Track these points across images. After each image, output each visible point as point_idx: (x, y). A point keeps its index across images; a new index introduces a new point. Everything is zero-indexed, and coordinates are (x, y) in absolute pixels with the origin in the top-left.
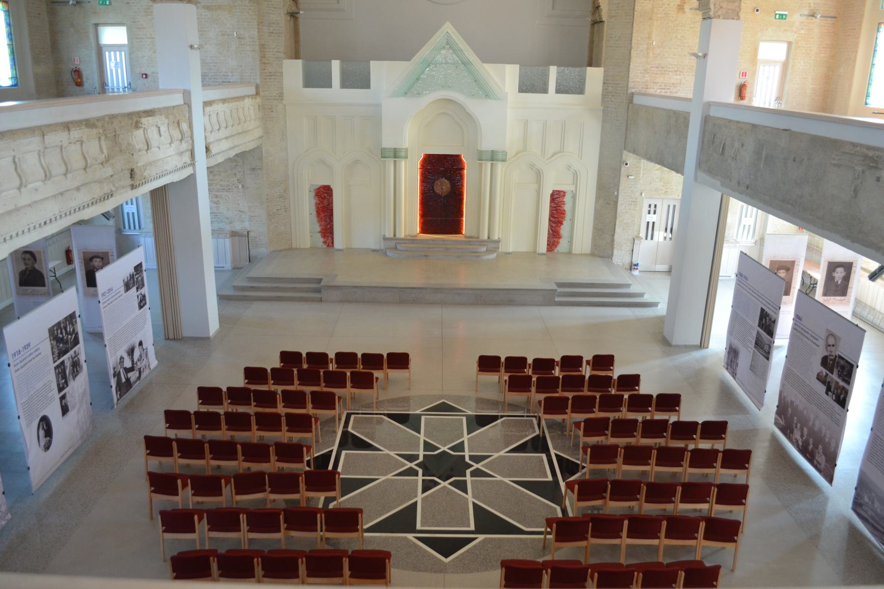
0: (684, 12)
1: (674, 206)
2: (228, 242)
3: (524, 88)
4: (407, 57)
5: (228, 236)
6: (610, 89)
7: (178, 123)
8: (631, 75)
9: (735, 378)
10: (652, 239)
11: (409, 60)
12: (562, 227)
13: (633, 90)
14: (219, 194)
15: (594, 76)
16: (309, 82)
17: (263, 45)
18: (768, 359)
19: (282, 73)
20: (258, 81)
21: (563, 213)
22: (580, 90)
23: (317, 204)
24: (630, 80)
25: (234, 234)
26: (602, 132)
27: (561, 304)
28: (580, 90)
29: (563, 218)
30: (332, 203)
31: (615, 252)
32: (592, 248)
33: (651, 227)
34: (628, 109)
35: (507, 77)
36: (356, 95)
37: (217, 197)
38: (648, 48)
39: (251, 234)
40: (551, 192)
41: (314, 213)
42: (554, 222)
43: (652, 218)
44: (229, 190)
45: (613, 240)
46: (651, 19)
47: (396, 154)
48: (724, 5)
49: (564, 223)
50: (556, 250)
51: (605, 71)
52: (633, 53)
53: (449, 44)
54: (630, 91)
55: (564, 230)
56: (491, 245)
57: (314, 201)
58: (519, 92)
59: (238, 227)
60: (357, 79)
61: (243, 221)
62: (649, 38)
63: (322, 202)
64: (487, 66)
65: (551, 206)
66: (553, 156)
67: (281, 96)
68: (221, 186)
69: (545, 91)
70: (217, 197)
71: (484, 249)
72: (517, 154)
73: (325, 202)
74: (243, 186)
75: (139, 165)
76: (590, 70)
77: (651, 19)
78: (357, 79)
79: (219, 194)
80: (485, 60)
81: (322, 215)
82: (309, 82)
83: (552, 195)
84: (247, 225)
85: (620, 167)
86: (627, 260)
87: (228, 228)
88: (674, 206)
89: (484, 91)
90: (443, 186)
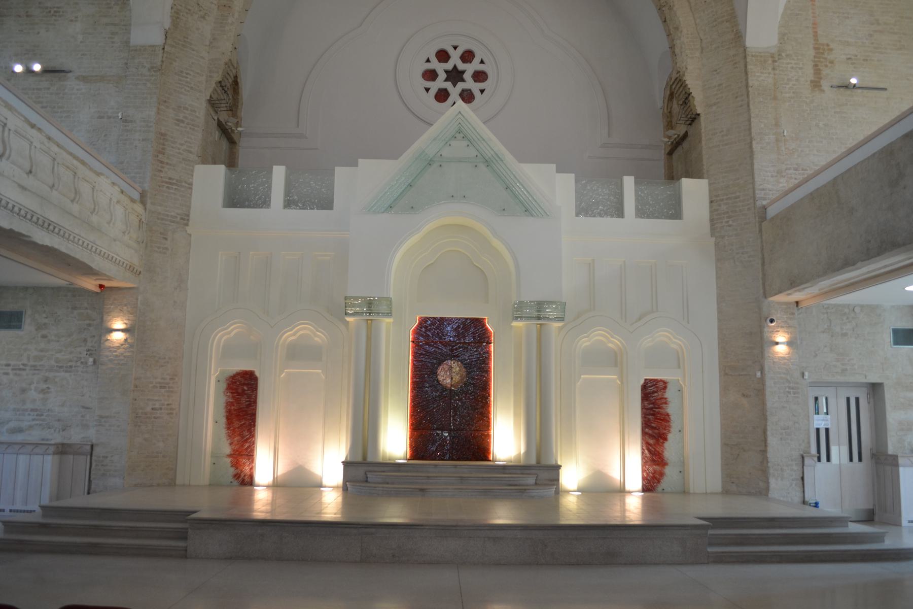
0: (823, 91)
1: (857, 399)
2: (49, 462)
3: (584, 209)
4: (396, 157)
5: (52, 449)
6: (724, 208)
10: (828, 460)
11: (397, 159)
12: (666, 444)
13: (764, 203)
14: (51, 375)
15: (694, 192)
16: (235, 199)
17: (162, 134)
19: (191, 184)
20: (147, 186)
22: (674, 211)
23: (229, 404)
24: (757, 186)
25: (63, 450)
26: (718, 278)
27: (720, 559)
28: (674, 211)
29: (668, 428)
30: (255, 402)
31: (772, 481)
32: (724, 482)
33: (824, 438)
34: (760, 231)
35: (556, 188)
36: (309, 219)
37: (46, 380)
38: (777, 140)
39: (97, 450)
40: (642, 382)
41: (223, 421)
42: (651, 436)
43: (820, 421)
46: (775, 98)
47: (372, 308)
49: (670, 437)
50: (659, 488)
51: (710, 184)
53: (461, 133)
54: (759, 203)
55: (670, 450)
56: (544, 475)
57: (223, 400)
58: (577, 215)
59: (75, 436)
60: (312, 196)
62: (777, 125)
63: (238, 401)
64: (523, 165)
65: (643, 408)
66: (640, 319)
67: (185, 219)
68: (57, 361)
69: (619, 212)
70: (46, 380)
71: (531, 480)
73: (244, 400)
74: (95, 362)
76: (687, 183)
77: (775, 98)
78: (312, 196)
79: (51, 375)
81: (237, 424)
82: (235, 199)
83: (644, 387)
84: (92, 434)
87: (57, 438)
88: (857, 399)
90: (450, 374)
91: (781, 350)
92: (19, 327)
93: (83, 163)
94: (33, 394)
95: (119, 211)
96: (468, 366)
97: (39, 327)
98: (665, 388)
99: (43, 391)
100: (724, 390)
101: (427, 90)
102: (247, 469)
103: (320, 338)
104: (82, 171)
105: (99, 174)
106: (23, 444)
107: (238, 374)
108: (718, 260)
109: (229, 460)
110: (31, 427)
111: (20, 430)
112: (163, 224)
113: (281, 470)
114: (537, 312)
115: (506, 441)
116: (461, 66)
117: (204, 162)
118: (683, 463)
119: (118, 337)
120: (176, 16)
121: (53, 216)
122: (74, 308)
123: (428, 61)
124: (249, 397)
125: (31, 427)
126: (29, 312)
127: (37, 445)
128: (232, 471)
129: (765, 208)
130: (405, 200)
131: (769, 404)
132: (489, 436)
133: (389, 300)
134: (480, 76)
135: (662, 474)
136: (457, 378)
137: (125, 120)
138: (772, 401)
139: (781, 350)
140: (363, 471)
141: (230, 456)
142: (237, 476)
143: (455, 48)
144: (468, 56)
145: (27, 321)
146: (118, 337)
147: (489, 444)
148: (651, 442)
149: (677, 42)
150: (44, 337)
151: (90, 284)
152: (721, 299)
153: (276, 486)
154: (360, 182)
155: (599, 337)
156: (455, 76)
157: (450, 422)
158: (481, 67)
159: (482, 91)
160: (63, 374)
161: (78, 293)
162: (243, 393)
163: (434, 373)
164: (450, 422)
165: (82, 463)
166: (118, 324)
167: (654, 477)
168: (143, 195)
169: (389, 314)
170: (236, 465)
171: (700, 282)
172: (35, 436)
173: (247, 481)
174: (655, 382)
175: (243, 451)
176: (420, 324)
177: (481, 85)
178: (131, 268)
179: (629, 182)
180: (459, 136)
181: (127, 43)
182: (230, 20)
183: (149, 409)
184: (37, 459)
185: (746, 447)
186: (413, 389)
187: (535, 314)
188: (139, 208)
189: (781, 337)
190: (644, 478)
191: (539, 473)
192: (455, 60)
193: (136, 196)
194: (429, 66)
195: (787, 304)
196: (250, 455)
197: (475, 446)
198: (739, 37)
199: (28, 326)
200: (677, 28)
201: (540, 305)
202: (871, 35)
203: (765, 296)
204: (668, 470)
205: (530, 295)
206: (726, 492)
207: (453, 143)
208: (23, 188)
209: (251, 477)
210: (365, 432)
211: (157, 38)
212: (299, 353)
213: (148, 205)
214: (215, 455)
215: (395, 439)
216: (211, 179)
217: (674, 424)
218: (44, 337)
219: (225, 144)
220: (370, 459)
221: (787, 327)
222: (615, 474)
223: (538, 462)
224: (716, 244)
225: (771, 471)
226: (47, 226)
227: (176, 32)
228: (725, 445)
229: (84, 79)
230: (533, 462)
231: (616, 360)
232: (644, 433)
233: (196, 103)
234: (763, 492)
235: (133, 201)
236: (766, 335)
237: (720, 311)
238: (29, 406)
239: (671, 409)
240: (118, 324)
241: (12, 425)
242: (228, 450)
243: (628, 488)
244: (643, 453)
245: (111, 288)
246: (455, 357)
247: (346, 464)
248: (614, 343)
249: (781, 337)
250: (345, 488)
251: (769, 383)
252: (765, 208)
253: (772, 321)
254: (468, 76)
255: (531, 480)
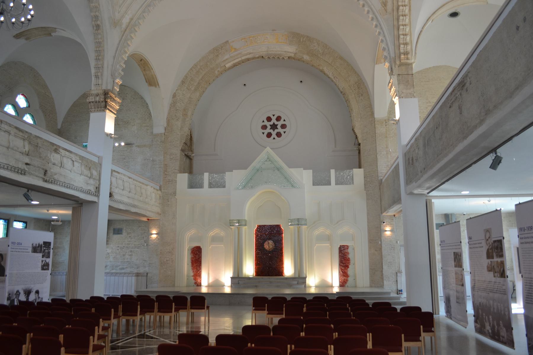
2: (134, 278)
4: (246, 168)
5: (134, 275)
7: (90, 168)
8: (379, 169)
9: (451, 318)
12: (349, 269)
16: (191, 186)
18: (463, 285)
20: (161, 183)
21: (348, 260)
22: (351, 181)
23: (192, 258)
25: (138, 275)
26: (367, 206)
28: (351, 181)
29: (349, 263)
30: (201, 257)
31: (385, 282)
34: (380, 189)
35: (305, 176)
37: (131, 251)
38: (387, 153)
40: (339, 246)
41: (190, 264)
42: (343, 266)
44: (138, 248)
45: (382, 275)
46: (386, 137)
48: (404, 91)
49: (350, 266)
50: (346, 285)
52: (379, 157)
53: (269, 159)
54: (380, 178)
55: (350, 271)
56: (300, 281)
57: (190, 256)
58: (313, 185)
59: (141, 270)
61: (145, 267)
62: (387, 147)
63: (195, 257)
64: (291, 169)
67: (175, 194)
69: (329, 183)
70: (131, 251)
71: (296, 282)
72: (314, 223)
73: (197, 256)
75: (52, 170)
80: (290, 167)
81: (195, 265)
82: (191, 186)
83: (340, 248)
84: (147, 269)
85: (380, 225)
86: (394, 288)
87: (135, 271)
89: (290, 183)
90: (269, 245)
91: (388, 233)
92: (121, 234)
93: (143, 184)
94: (127, 256)
95: (153, 195)
96: (275, 242)
97: (128, 234)
98: (348, 248)
99: (130, 255)
100: (370, 248)
101: (263, 133)
102: (199, 281)
103: (222, 234)
104: (143, 186)
105: (147, 185)
106: (125, 273)
107: (195, 247)
108: (367, 199)
109: (193, 278)
110: (127, 268)
111: (123, 269)
112: (167, 197)
113: (211, 281)
114: (299, 222)
115: (288, 269)
116: (276, 123)
117: (180, 173)
118: (355, 276)
119: (154, 236)
120: (168, 121)
121: (136, 203)
122: (139, 227)
123: (263, 122)
124: (199, 255)
125: (127, 268)
126: (125, 228)
127: (130, 273)
128: (194, 281)
129: (382, 180)
130: (249, 184)
131: (383, 254)
132: (283, 267)
133: (245, 220)
134: (284, 126)
135: (347, 280)
136: (271, 247)
137: (153, 161)
138: (384, 253)
139: (388, 233)
140: (238, 280)
141: (193, 276)
142: (196, 283)
143: (274, 115)
144: (278, 119)
145: (124, 231)
146: (154, 236)
147: (283, 270)
148: (343, 268)
149: (352, 115)
150: (130, 237)
151: (145, 219)
152: (368, 214)
153: (209, 286)
154: (234, 178)
155: (320, 231)
156: (274, 127)
157: (269, 263)
158: (284, 123)
159: (285, 132)
160: (136, 249)
161: (140, 221)
162: (196, 254)
163: (262, 245)
164: (269, 263)
165: (144, 278)
166: (154, 232)
167: (344, 282)
168: (160, 187)
169: (245, 225)
170: (195, 279)
171: (360, 207)
172: (128, 270)
173: (199, 285)
174: (344, 246)
175: (197, 274)
176: (257, 228)
177: (284, 130)
178: (158, 213)
179: (333, 172)
180: (268, 160)
181: (152, 132)
182: (187, 119)
183: (165, 260)
184: (130, 278)
185: (376, 269)
186: (256, 249)
187: (297, 223)
188: (159, 192)
189: (388, 228)
190: (340, 282)
191: (300, 279)
192: (274, 120)
193: (158, 188)
194: (264, 124)
195: (390, 216)
196: (200, 276)
197: (279, 272)
198: (373, 114)
199: (124, 233)
200: (352, 110)
201: (298, 220)
202: (427, 108)
203: (382, 213)
204: (349, 279)
205: (294, 216)
206: (371, 287)
207: (266, 163)
208: (129, 197)
209: (200, 283)
210: (238, 267)
211: (162, 131)
212: (216, 239)
213: (162, 190)
214: (188, 276)
215: (249, 269)
216: (183, 179)
217: (352, 262)
218: (130, 237)
219: (188, 160)
220: (240, 276)
221: (390, 224)
222: (329, 280)
223: (299, 276)
224: (366, 193)
225: (384, 278)
226: (135, 206)
227: (169, 127)
228: (370, 269)
229: (138, 146)
230: (297, 276)
231: (329, 239)
232: (340, 265)
233: (177, 152)
234: (382, 286)
235: (157, 190)
236: (382, 228)
237: (368, 219)
238: (126, 260)
239: (350, 256)
240: (154, 232)
241: (120, 267)
242: (192, 274)
243: (334, 285)
244: (340, 272)
245: (151, 220)
246: (270, 239)
247: (232, 278)
248: (328, 232)
249: (388, 228)
250: (231, 286)
251: (383, 245)
252: (382, 180)
253: (384, 223)
254: (279, 127)
255: (296, 282)
